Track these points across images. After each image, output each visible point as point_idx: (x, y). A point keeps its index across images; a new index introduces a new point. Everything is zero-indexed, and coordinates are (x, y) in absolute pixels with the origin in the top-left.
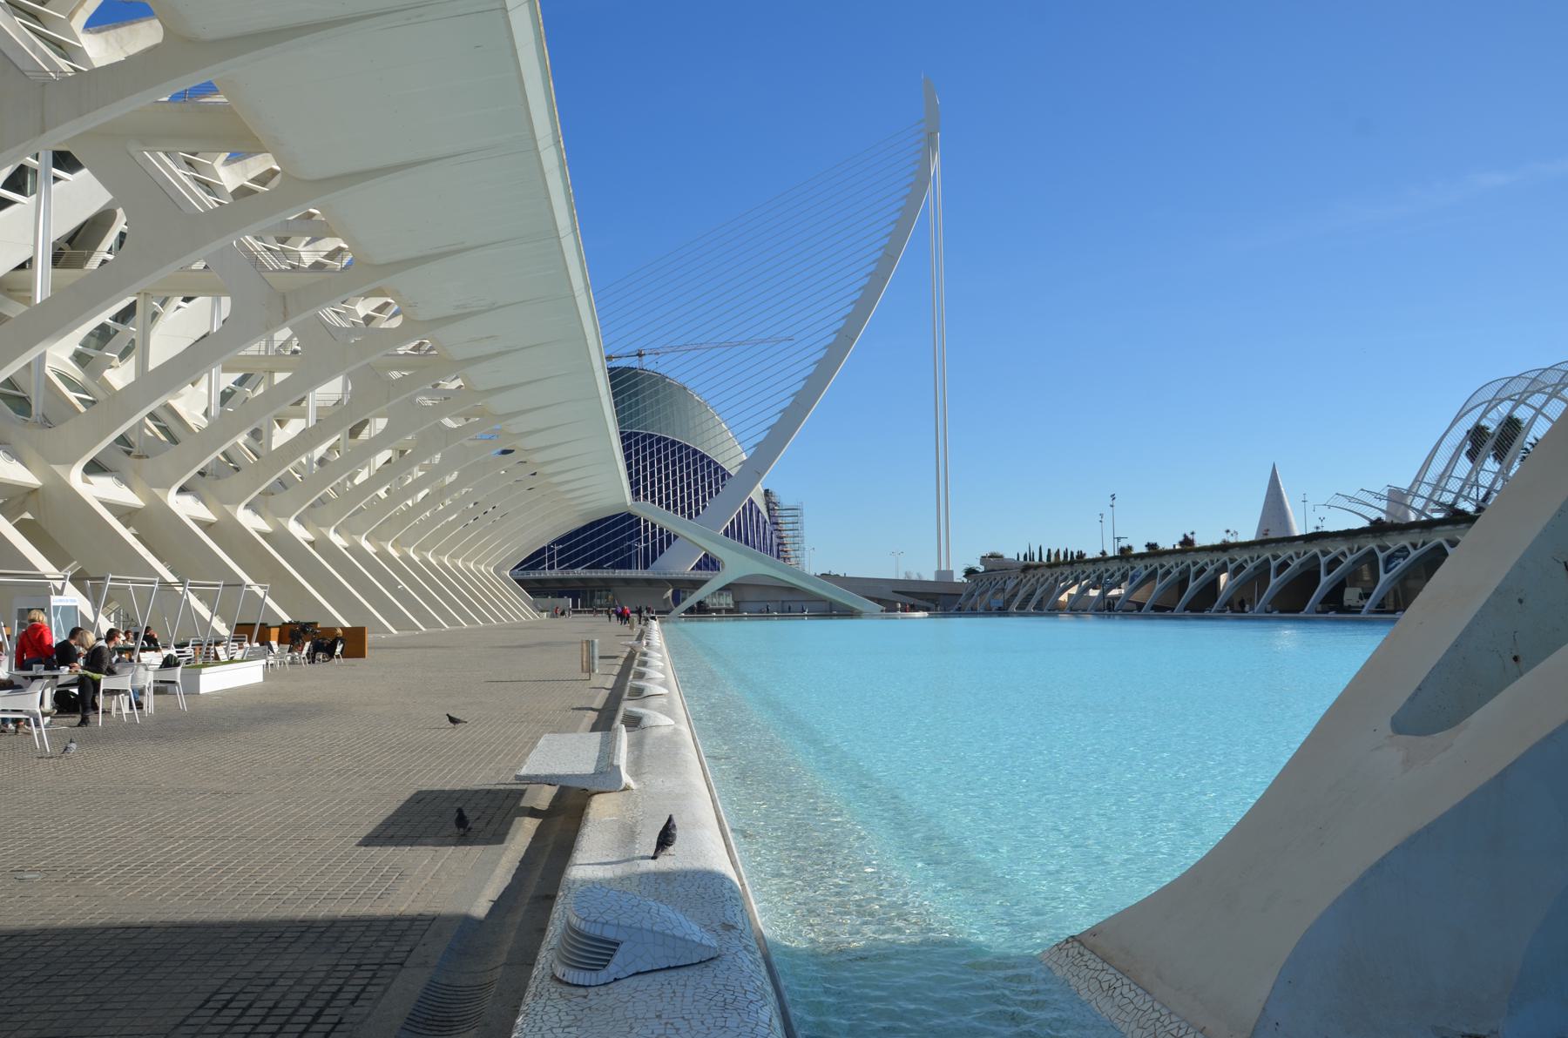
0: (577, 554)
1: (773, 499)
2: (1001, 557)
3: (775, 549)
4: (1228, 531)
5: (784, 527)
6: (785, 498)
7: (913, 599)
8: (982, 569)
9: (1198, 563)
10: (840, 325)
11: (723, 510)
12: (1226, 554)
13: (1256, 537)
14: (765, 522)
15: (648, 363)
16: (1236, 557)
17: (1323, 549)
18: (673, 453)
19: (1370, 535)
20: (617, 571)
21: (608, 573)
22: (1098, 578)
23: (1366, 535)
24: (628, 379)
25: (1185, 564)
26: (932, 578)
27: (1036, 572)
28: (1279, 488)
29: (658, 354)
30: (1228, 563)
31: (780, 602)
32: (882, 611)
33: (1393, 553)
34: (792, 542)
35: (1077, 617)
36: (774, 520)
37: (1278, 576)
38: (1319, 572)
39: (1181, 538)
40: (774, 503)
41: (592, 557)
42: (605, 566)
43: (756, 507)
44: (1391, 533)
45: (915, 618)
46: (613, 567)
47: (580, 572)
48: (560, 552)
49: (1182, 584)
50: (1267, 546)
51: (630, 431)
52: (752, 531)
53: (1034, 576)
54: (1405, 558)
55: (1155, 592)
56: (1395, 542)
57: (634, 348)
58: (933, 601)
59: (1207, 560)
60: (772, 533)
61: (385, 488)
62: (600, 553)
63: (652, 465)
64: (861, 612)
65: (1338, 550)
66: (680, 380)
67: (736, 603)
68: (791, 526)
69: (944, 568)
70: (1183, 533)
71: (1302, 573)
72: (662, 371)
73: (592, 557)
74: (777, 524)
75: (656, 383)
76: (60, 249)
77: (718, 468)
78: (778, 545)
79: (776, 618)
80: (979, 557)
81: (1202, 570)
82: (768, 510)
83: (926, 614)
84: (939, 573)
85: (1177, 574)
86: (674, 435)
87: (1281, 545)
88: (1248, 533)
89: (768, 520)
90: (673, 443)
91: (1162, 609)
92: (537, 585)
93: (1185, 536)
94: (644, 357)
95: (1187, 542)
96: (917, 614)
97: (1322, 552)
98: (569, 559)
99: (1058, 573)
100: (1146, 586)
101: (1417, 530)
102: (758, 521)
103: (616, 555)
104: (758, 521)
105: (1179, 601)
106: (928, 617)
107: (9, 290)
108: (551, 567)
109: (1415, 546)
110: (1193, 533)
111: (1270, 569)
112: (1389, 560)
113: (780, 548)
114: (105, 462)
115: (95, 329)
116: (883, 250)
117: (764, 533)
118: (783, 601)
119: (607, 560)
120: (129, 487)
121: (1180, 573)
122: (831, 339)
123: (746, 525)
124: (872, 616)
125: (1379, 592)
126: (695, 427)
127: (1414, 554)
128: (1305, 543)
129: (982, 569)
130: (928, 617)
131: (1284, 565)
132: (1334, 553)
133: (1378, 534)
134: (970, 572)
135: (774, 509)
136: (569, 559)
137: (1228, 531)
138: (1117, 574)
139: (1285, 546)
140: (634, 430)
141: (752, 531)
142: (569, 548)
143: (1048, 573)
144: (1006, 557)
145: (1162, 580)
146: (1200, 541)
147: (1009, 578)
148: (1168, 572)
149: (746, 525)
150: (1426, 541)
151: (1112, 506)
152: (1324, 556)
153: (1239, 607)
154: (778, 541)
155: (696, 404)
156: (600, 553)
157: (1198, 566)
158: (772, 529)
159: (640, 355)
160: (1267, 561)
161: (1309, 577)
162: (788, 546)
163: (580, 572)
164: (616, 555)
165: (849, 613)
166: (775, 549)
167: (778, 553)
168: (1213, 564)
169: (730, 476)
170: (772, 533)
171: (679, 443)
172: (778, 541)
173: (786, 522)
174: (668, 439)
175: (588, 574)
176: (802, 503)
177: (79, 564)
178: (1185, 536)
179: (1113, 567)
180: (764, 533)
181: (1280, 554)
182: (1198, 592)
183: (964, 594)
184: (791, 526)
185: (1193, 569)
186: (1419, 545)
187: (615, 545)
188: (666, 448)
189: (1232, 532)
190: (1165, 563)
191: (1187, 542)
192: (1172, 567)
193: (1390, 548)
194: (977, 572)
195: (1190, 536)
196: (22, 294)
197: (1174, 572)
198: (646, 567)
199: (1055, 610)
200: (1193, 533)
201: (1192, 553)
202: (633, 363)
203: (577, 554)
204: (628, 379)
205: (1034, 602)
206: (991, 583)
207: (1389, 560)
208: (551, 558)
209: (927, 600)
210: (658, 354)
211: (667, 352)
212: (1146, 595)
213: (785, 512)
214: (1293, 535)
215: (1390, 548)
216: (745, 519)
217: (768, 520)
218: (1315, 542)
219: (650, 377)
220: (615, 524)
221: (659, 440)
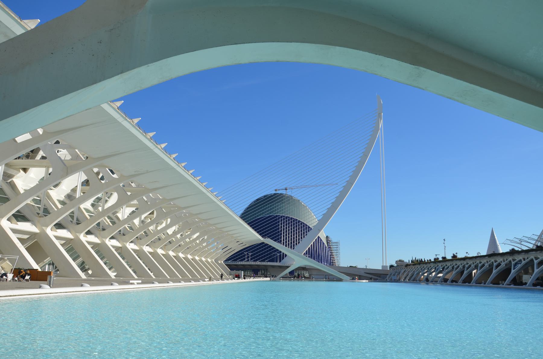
0: (257, 256)
1: (329, 240)
2: (403, 261)
3: (329, 256)
4: (467, 253)
5: (333, 249)
6: (333, 239)
7: (371, 275)
8: (396, 265)
9: (468, 263)
10: (348, 179)
11: (307, 243)
12: (465, 261)
13: (487, 254)
14: (326, 247)
15: (289, 192)
16: (469, 262)
17: (495, 260)
18: (291, 222)
19: (509, 255)
20: (268, 263)
21: (254, 263)
22: (452, 268)
23: (507, 255)
24: (280, 198)
25: (508, 260)
26: (381, 269)
27: (410, 267)
28: (494, 237)
29: (292, 189)
30: (512, 261)
31: (325, 276)
32: (350, 279)
33: (517, 262)
34: (336, 252)
35: (420, 284)
36: (329, 246)
37: (496, 269)
38: (511, 269)
39: (452, 255)
40: (329, 241)
41: (262, 257)
42: (266, 261)
43: (323, 242)
44: (515, 254)
45: (363, 282)
46: (269, 261)
47: (258, 263)
48: (251, 256)
49: (490, 271)
50: (477, 258)
51: (282, 215)
52: (321, 250)
53: (409, 268)
54: (521, 264)
55: (452, 275)
56: (518, 258)
57: (284, 187)
58: (379, 277)
59: (501, 260)
60: (328, 251)
61: (180, 234)
62: (265, 256)
63: (289, 227)
64: (343, 280)
65: (519, 259)
66: (299, 198)
67: (310, 275)
68: (335, 249)
69: (384, 265)
70: (453, 253)
71: (505, 269)
72: (292, 195)
73: (262, 257)
74: (330, 248)
75: (289, 200)
76: (29, 153)
77: (309, 227)
78: (331, 255)
79: (303, 280)
80: (395, 261)
81: (499, 265)
82: (327, 243)
83: (367, 281)
84: (383, 266)
85: (488, 266)
86: (292, 216)
87: (481, 258)
88: (484, 252)
89: (327, 247)
90: (292, 218)
91: (454, 281)
92: (257, 267)
93: (453, 254)
94: (287, 190)
95: (454, 257)
96: (364, 281)
97: (513, 259)
98: (254, 258)
99: (445, 265)
100: (450, 273)
101: (524, 253)
102: (323, 247)
103: (270, 257)
104: (323, 247)
105: (461, 277)
106: (368, 282)
107: (11, 166)
108: (248, 261)
109: (524, 259)
110: (456, 253)
111: (534, 264)
112: (516, 265)
113: (331, 256)
114: (63, 224)
115: (40, 180)
116: (363, 153)
117: (326, 251)
118: (326, 275)
119: (267, 259)
120: (71, 233)
121: (506, 265)
122: (345, 184)
123: (319, 248)
124: (346, 281)
125: (510, 278)
126: (302, 215)
127: (523, 262)
128: (489, 257)
129: (396, 265)
130: (368, 282)
131: (499, 265)
132: (499, 261)
133: (511, 255)
134: (391, 266)
135: (329, 243)
136: (254, 258)
137: (467, 253)
138: (450, 267)
139: (482, 258)
140: (283, 215)
141: (321, 250)
142: (254, 254)
143: (413, 267)
144: (405, 261)
145: (481, 269)
146: (459, 256)
147: (403, 269)
148: (483, 265)
149: (319, 248)
150: (528, 257)
151: (444, 243)
152: (536, 260)
153: (481, 282)
154: (330, 254)
155: (303, 206)
156: (265, 256)
157: (497, 263)
158: (328, 250)
159: (286, 189)
160: (510, 262)
161: (507, 271)
162: (334, 256)
163: (258, 263)
164: (270, 257)
165: (340, 280)
166: (329, 256)
167: (330, 258)
168: (487, 263)
169: (311, 229)
170: (328, 251)
171: (294, 218)
172: (330, 254)
173: (333, 247)
174: (290, 217)
175: (272, 264)
176: (339, 241)
177: (82, 258)
178: (453, 254)
179: (432, 265)
180: (326, 251)
181: (540, 257)
182: (468, 275)
183: (389, 274)
184: (335, 249)
185: (495, 264)
186: (526, 259)
187: (270, 254)
188: (289, 220)
189: (468, 253)
190: (447, 264)
191: (454, 257)
192: (485, 263)
193: (539, 258)
194: (394, 266)
195: (456, 255)
196: (14, 167)
197: (502, 264)
198: (280, 261)
199: (420, 281)
200: (456, 253)
201: (455, 261)
202: (284, 192)
203: (257, 256)
204: (280, 198)
205: (408, 278)
206: (422, 269)
207: (516, 265)
208: (248, 257)
209: (377, 276)
210: (292, 189)
211: (295, 189)
212: (450, 276)
213: (333, 244)
214: (499, 253)
215: (539, 258)
216: (316, 244)
217: (327, 247)
218: (492, 257)
219: (288, 197)
220: (255, 247)
221: (287, 217)
